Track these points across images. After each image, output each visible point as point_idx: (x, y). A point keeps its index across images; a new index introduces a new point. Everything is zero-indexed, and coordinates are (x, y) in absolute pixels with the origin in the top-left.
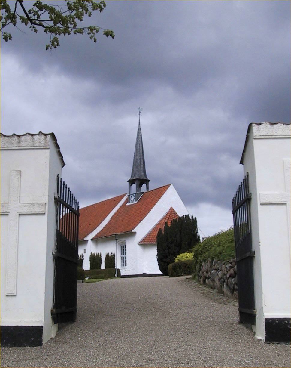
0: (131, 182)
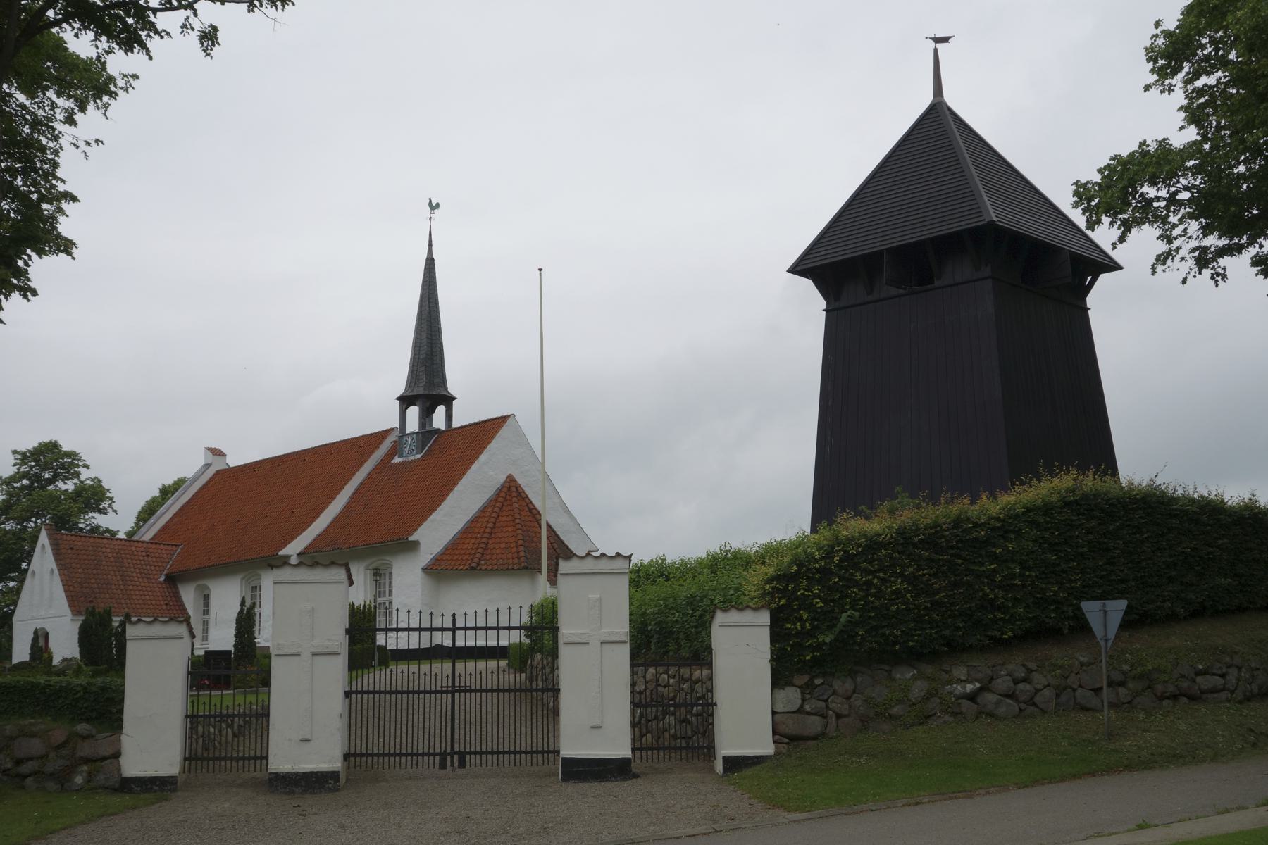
0: (406, 401)
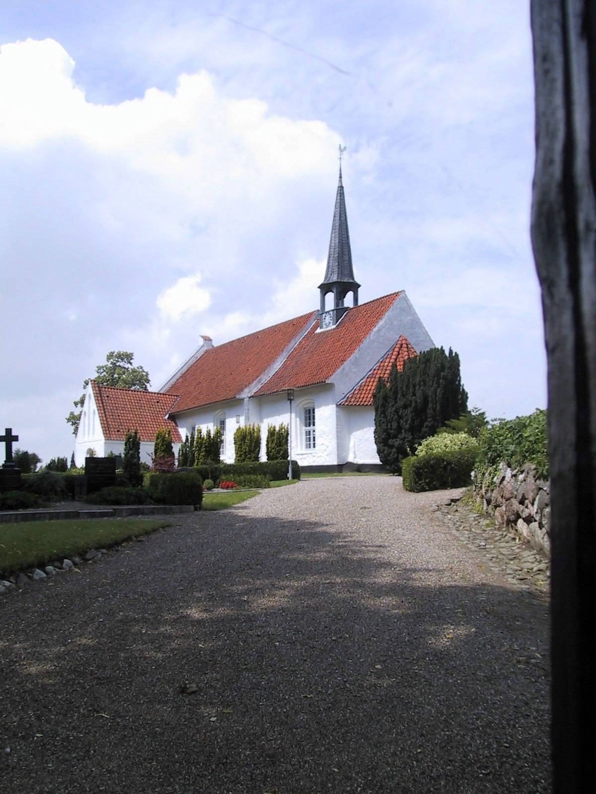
0: (325, 288)
